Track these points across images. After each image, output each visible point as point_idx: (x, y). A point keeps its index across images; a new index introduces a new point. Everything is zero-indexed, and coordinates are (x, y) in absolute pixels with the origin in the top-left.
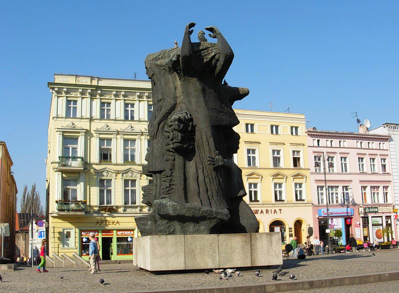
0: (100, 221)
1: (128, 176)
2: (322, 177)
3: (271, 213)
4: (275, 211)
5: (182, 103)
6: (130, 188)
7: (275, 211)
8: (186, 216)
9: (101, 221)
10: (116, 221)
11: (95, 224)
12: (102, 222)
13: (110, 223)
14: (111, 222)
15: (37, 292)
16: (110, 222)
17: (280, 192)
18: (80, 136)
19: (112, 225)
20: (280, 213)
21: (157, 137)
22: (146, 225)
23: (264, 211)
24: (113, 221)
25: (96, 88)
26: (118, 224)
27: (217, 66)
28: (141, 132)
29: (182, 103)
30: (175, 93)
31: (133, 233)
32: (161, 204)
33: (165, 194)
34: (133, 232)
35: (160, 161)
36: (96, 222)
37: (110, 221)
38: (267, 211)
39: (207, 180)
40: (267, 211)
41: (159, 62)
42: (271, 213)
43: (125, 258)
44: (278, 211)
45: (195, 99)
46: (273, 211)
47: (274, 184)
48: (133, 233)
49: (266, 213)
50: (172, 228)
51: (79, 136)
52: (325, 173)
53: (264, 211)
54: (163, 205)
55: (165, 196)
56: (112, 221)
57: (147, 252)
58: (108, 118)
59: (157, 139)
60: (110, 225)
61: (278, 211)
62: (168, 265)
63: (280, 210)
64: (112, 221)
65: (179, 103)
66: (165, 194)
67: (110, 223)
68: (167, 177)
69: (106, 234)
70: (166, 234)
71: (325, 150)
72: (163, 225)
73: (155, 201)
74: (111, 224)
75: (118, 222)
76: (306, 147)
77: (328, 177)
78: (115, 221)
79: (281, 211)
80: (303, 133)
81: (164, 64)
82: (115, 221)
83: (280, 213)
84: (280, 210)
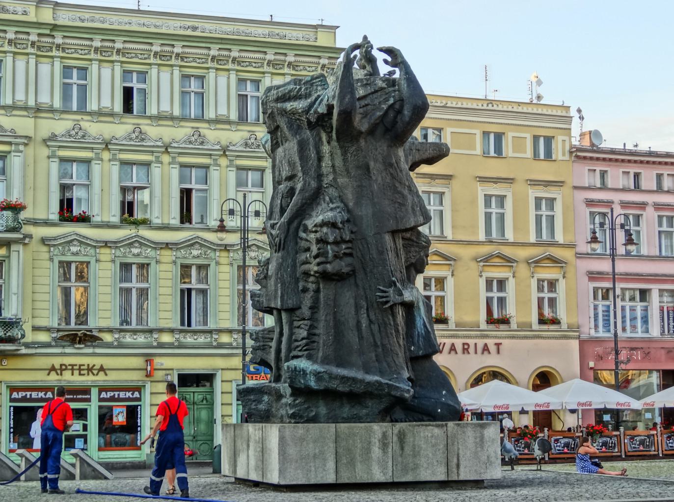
0: (57, 366)
1: (133, 256)
2: (605, 266)
3: (476, 353)
4: (486, 349)
5: (331, 186)
6: (135, 284)
7: (486, 349)
8: (339, 391)
9: (61, 365)
10: (97, 367)
11: (47, 371)
12: (64, 367)
13: (83, 370)
14: (86, 367)
15: (258, 501)
16: (82, 367)
17: (502, 301)
18: (13, 154)
19: (88, 374)
20: (498, 352)
21: (286, 247)
22: (260, 402)
23: (459, 348)
24: (90, 366)
25: (51, 30)
26: (102, 373)
27: (397, 122)
28: (162, 145)
29: (331, 186)
30: (319, 166)
31: (138, 396)
32: (298, 368)
33: (300, 351)
34: (140, 394)
35: (292, 290)
36: (50, 367)
37: (84, 365)
38: (466, 349)
39: (375, 328)
40: (466, 347)
41: (289, 106)
42: (476, 353)
43: (112, 457)
44: (493, 349)
45: (356, 181)
46: (480, 350)
47: (487, 281)
48: (138, 396)
49: (464, 353)
50: (312, 411)
51: (9, 152)
52: (613, 256)
53: (459, 348)
54: (300, 372)
55: (300, 354)
56: (88, 365)
57: (264, 451)
58: (82, 110)
59: (285, 249)
60: (84, 375)
61: (493, 349)
62: (307, 474)
63: (498, 345)
64: (88, 365)
65: (325, 186)
66: (300, 351)
67: (83, 370)
68: (304, 319)
69: (72, 396)
70: (302, 421)
71: (617, 197)
72: (297, 404)
73: (286, 364)
74: (85, 372)
75: (102, 369)
76: (567, 190)
77: (622, 267)
78: (94, 365)
79: (501, 347)
80: (564, 155)
81: (300, 111)
82: (94, 365)
83: (498, 352)
84: (498, 345)
